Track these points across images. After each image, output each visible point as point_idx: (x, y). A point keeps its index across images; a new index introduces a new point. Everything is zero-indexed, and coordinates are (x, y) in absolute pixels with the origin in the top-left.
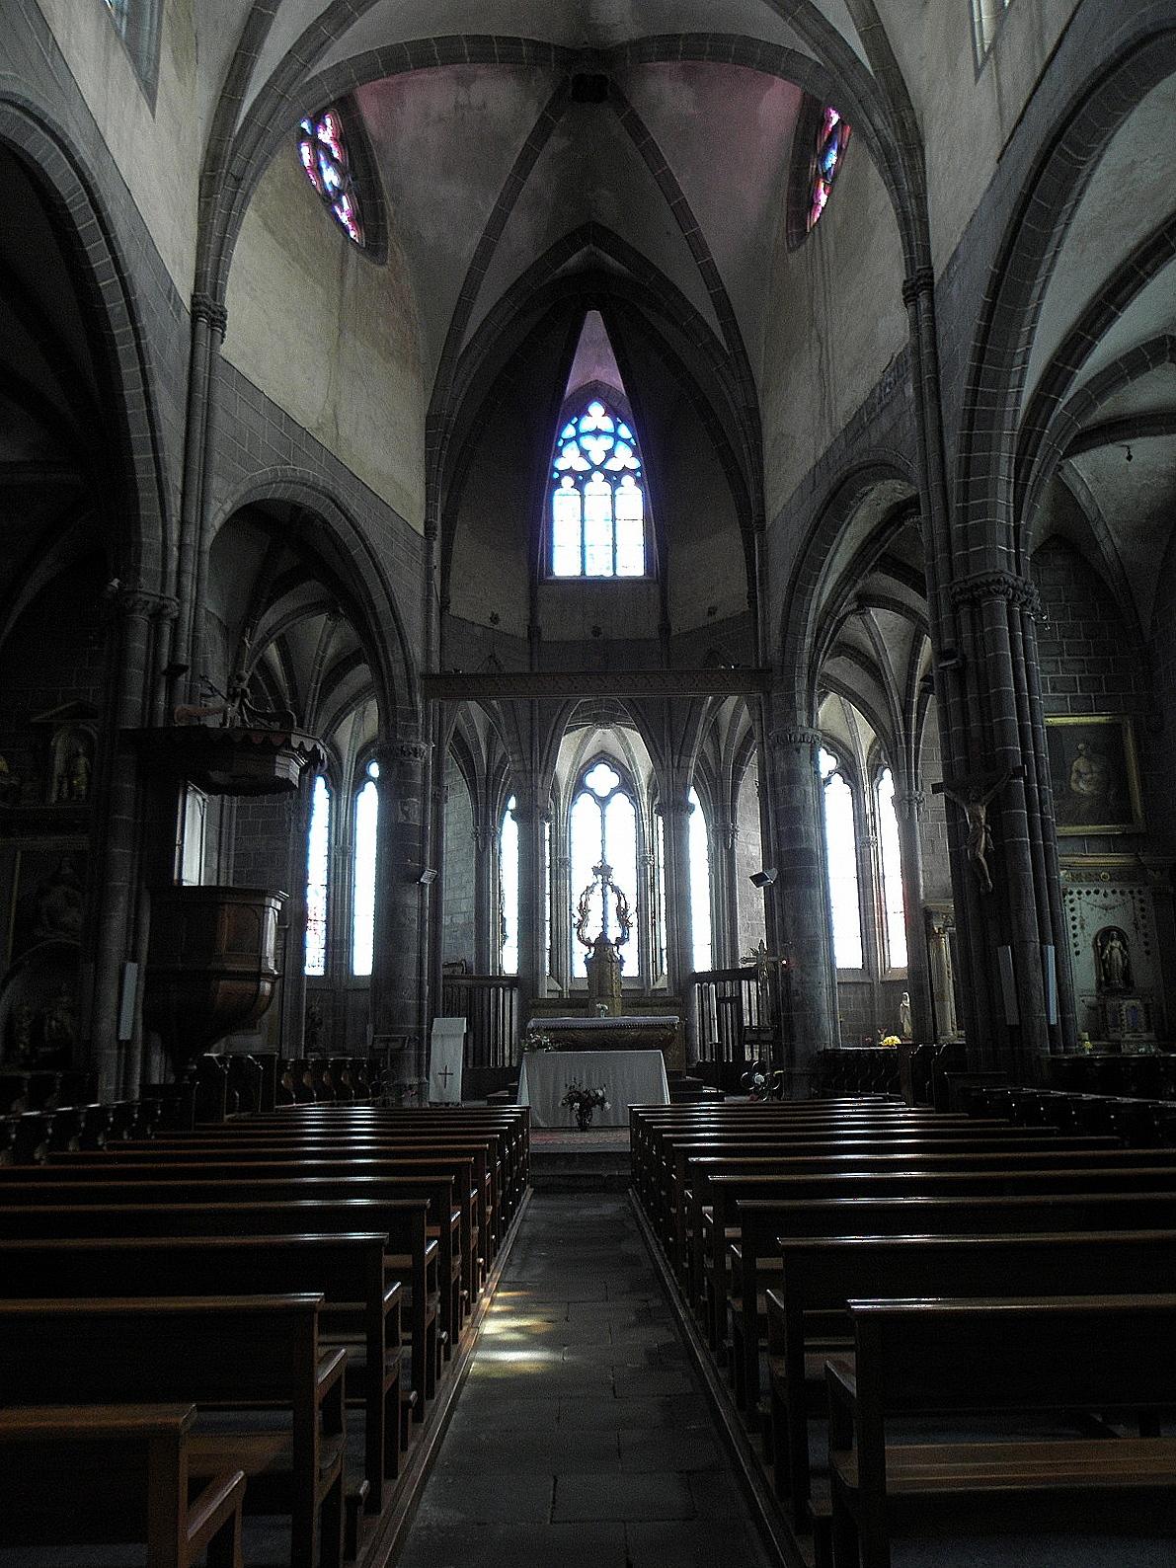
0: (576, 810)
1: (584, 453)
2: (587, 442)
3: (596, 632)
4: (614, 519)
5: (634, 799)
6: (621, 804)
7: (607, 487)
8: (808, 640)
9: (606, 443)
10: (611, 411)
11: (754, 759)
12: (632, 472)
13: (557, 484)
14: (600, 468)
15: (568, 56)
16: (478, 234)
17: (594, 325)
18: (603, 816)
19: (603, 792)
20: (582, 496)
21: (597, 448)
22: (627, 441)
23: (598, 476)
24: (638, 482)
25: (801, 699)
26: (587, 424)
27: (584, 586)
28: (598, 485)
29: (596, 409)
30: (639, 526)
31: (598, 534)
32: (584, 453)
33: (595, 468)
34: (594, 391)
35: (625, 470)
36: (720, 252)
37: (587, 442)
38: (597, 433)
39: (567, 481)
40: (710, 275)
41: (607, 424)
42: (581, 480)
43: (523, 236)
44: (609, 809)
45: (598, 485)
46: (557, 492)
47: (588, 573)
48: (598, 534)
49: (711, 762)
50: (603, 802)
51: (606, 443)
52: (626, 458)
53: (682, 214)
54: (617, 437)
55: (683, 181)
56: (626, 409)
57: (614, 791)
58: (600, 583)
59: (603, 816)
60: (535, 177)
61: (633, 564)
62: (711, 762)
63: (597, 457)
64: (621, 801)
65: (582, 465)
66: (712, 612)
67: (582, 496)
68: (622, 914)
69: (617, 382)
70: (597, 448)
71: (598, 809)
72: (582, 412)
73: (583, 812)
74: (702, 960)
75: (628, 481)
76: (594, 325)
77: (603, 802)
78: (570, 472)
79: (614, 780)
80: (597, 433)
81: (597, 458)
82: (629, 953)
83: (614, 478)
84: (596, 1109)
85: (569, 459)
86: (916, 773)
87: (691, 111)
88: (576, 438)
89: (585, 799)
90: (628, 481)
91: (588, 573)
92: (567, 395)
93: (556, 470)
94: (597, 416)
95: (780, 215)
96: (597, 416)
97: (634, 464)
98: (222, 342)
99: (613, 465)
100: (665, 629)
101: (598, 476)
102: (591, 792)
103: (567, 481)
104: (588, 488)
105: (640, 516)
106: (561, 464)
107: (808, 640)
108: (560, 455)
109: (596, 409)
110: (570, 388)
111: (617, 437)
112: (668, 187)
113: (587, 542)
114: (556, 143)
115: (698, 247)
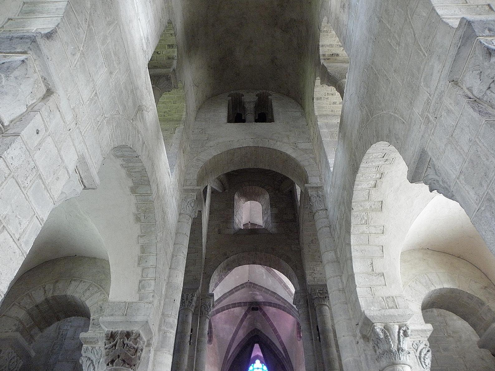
10: (261, 362)
15: (251, 303)
16: (232, 335)
17: (257, 346)
34: (257, 357)
36: (284, 339)
40: (282, 343)
43: (241, 334)
53: (275, 331)
55: (275, 324)
60: (244, 323)
69: (261, 354)
72: (254, 363)
76: (257, 346)
86: (103, 56)
87: (275, 311)
92: (251, 358)
95: (295, 332)
98: (338, 55)
110: (252, 356)
112: (272, 325)
114: (248, 316)
115: (279, 337)
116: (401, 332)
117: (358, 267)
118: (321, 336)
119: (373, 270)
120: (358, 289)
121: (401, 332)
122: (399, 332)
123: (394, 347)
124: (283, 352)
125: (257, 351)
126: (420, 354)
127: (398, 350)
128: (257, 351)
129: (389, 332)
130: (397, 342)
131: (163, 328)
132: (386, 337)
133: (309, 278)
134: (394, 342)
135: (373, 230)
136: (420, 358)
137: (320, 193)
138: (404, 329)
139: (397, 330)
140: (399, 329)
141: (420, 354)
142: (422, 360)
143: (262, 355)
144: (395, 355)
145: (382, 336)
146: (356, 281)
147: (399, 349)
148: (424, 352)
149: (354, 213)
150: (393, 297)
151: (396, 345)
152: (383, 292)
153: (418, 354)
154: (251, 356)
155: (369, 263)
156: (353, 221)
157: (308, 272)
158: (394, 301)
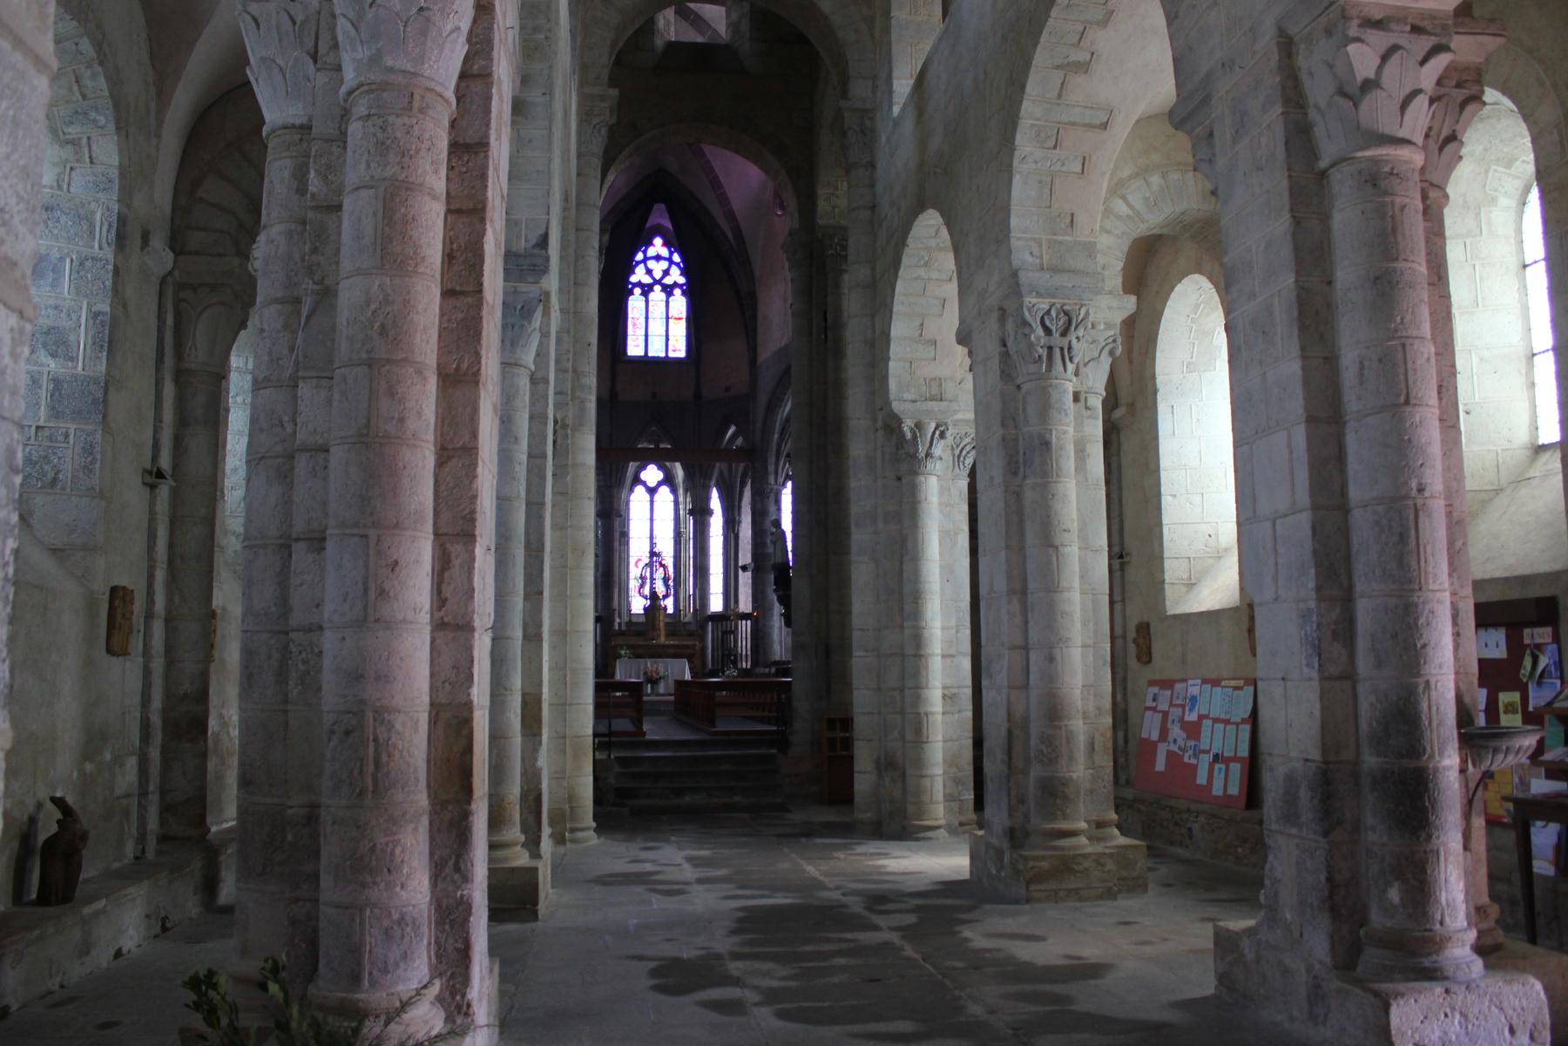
0: (633, 497)
1: (649, 272)
2: (651, 264)
3: (654, 395)
4: (667, 318)
5: (674, 491)
6: (664, 493)
7: (663, 296)
8: (776, 436)
9: (664, 265)
11: (749, 484)
12: (680, 286)
13: (631, 293)
14: (659, 282)
18: (652, 502)
19: (652, 484)
20: (647, 301)
21: (658, 268)
22: (677, 265)
23: (657, 288)
24: (684, 293)
25: (771, 468)
26: (651, 252)
27: (646, 362)
28: (657, 295)
29: (658, 241)
30: (683, 324)
31: (657, 327)
32: (649, 272)
33: (657, 282)
34: (658, 231)
35: (676, 285)
37: (651, 264)
38: (658, 258)
39: (637, 291)
40: (730, 215)
41: (664, 252)
42: (646, 290)
44: (657, 497)
45: (657, 295)
46: (630, 298)
47: (650, 354)
48: (657, 327)
49: (726, 475)
50: (652, 491)
51: (664, 265)
52: (676, 276)
54: (671, 262)
56: (676, 243)
57: (660, 484)
58: (657, 360)
59: (652, 502)
61: (679, 349)
62: (726, 475)
63: (658, 275)
64: (664, 491)
65: (647, 280)
66: (728, 389)
67: (647, 301)
68: (666, 580)
70: (658, 268)
71: (647, 497)
72: (650, 244)
73: (639, 497)
74: (716, 604)
75: (677, 292)
77: (652, 491)
78: (639, 284)
79: (660, 475)
80: (658, 258)
81: (657, 275)
82: (669, 604)
83: (668, 290)
84: (446, 620)
85: (639, 275)
88: (644, 261)
89: (639, 490)
90: (677, 292)
91: (650, 354)
93: (631, 283)
94: (658, 246)
96: (658, 246)
97: (682, 280)
99: (668, 281)
100: (698, 395)
101: (657, 288)
102: (644, 484)
103: (637, 291)
104: (652, 296)
105: (684, 315)
106: (633, 279)
107: (776, 436)
108: (634, 273)
109: (658, 241)
111: (671, 262)
113: (649, 333)
115: (724, 201)
116: (937, 433)
117: (900, 329)
118: (829, 334)
119: (921, 335)
120: (891, 364)
121: (937, 433)
122: (934, 433)
123: (922, 454)
124: (730, 235)
125: (660, 216)
126: (961, 451)
127: (926, 457)
128: (660, 216)
129: (920, 431)
130: (928, 445)
131: (578, 394)
132: (915, 437)
133: (822, 206)
134: (923, 445)
135: (935, 275)
136: (959, 456)
137: (868, 123)
138: (942, 429)
139: (932, 430)
140: (936, 429)
141: (961, 451)
142: (962, 459)
143: (670, 227)
144: (920, 461)
145: (909, 436)
146: (891, 351)
147: (928, 455)
148: (968, 448)
149: (907, 251)
150: (940, 379)
151: (926, 449)
152: (929, 370)
153: (957, 452)
154: (645, 224)
155: (918, 324)
156: (905, 260)
157: (822, 192)
158: (940, 385)
